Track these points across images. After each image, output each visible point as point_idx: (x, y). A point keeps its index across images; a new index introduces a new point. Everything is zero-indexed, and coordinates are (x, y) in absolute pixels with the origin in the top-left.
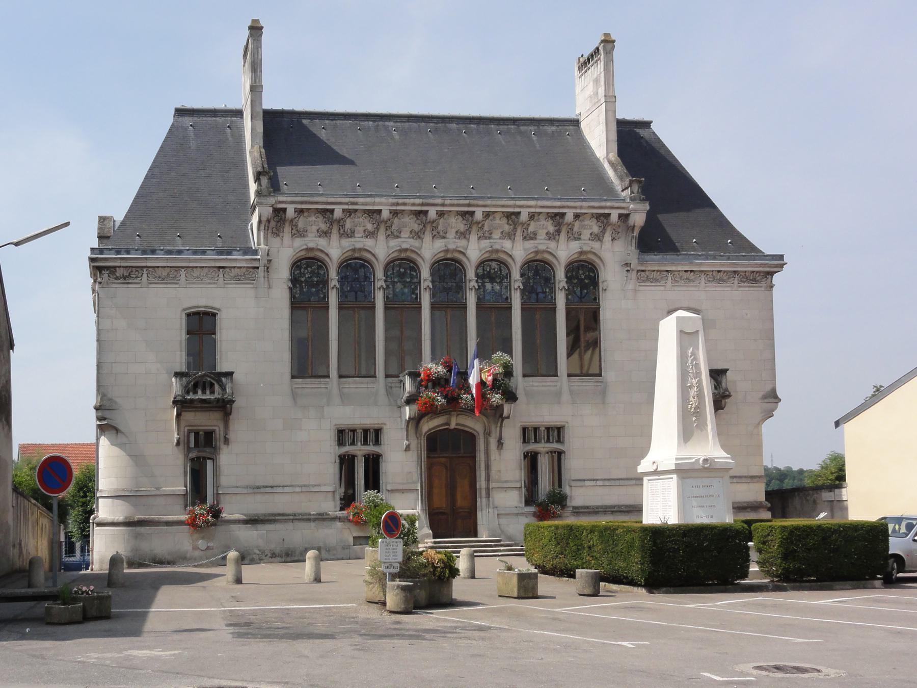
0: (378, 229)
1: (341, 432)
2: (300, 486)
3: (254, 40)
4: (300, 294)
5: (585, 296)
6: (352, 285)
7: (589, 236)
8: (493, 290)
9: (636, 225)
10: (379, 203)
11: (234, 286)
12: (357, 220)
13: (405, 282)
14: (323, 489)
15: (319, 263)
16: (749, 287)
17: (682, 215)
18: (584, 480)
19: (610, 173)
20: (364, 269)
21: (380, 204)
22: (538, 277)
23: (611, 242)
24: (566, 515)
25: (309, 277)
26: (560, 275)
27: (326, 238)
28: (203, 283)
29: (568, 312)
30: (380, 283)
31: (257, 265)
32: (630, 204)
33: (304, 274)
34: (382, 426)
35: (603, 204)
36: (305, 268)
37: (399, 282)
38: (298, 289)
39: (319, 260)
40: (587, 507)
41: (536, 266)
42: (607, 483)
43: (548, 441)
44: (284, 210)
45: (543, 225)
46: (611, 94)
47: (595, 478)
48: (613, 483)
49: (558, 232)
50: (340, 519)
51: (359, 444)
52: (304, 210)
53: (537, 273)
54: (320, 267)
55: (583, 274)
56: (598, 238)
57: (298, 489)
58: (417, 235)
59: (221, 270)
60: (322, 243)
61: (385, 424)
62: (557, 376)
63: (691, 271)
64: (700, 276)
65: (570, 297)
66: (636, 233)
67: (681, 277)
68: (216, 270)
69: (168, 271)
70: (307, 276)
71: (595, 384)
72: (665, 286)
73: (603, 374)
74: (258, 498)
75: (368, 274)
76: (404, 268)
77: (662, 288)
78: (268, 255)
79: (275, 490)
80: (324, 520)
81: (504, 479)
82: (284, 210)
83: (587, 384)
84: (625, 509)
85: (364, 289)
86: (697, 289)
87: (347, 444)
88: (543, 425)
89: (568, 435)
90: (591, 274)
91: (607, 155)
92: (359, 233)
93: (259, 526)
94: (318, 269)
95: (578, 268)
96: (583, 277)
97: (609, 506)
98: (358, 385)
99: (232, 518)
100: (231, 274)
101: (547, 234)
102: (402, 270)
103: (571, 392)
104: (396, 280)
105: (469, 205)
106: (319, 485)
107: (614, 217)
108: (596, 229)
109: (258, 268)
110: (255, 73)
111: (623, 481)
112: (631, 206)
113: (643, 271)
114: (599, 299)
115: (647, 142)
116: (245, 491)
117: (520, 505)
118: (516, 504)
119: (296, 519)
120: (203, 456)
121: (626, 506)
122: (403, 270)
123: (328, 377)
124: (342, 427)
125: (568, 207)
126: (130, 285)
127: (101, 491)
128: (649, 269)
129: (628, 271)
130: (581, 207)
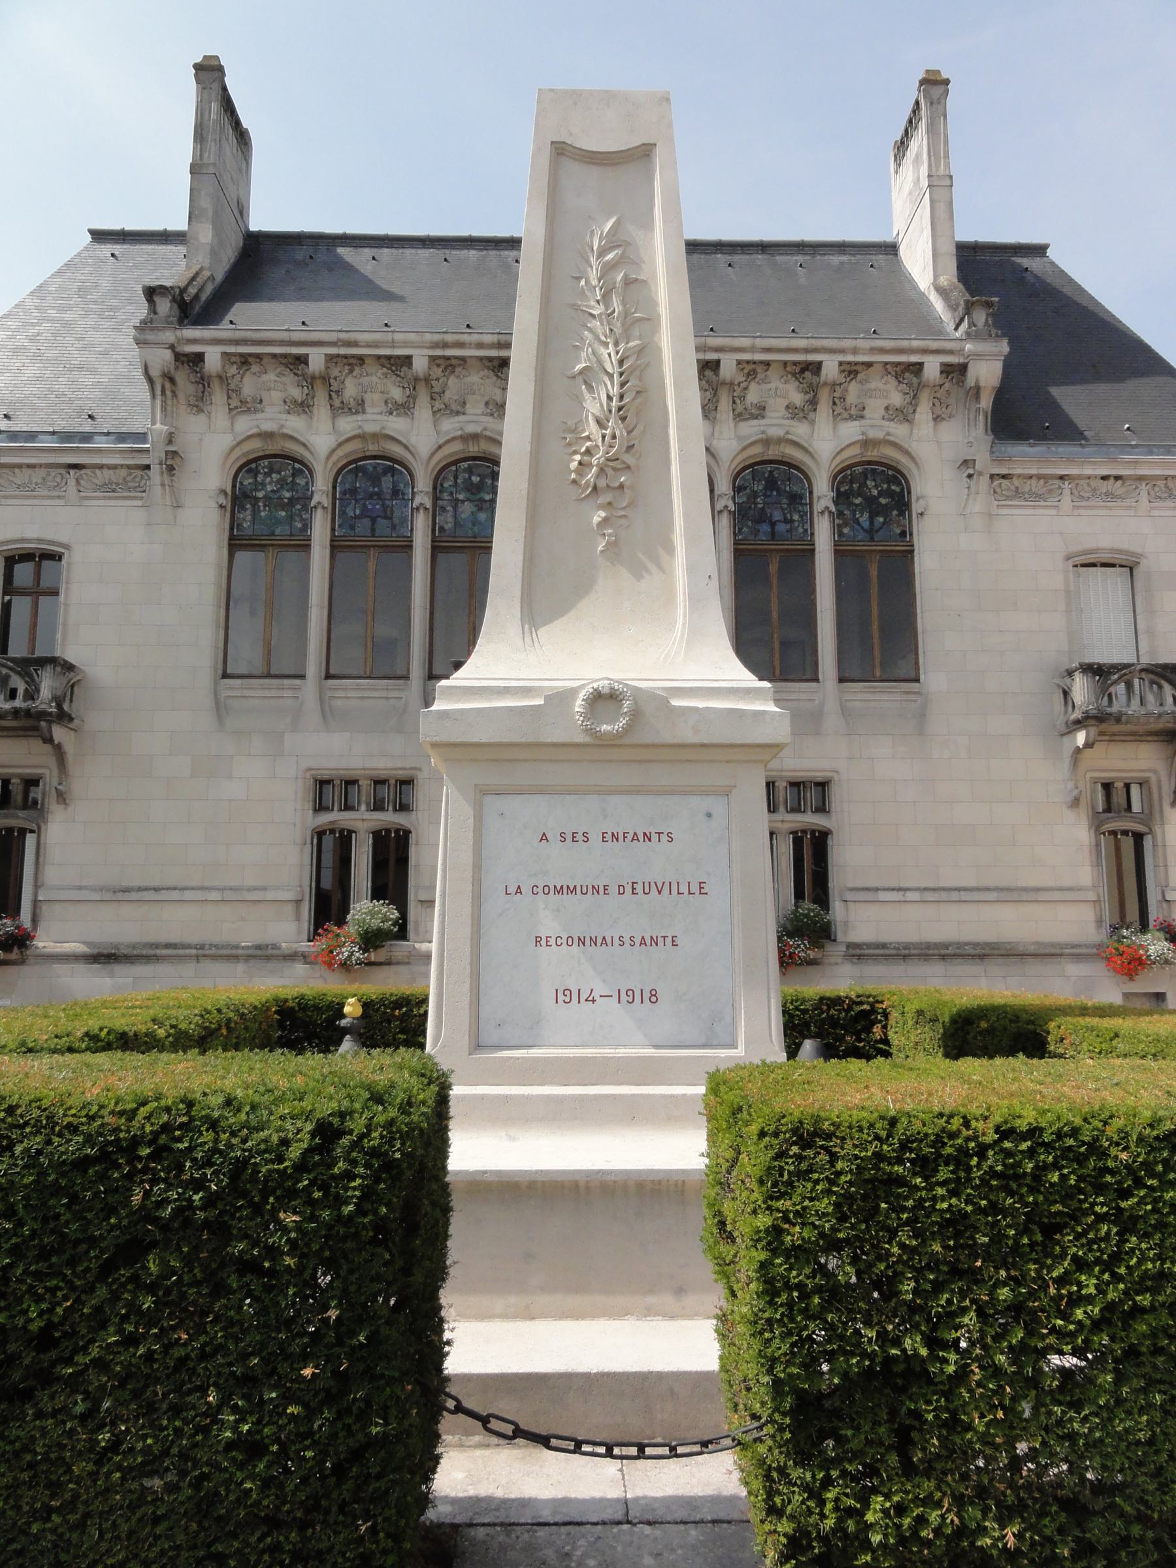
0: (412, 398)
1: (322, 784)
2: (219, 889)
3: (204, 88)
4: (253, 522)
6: (364, 505)
7: (883, 412)
9: (982, 384)
10: (405, 342)
11: (101, 502)
12: (365, 380)
13: (482, 500)
15: (297, 466)
17: (1102, 388)
18: (877, 889)
19: (938, 305)
20: (393, 476)
21: (406, 345)
22: (775, 493)
23: (931, 424)
24: (832, 960)
25: (273, 491)
26: (823, 491)
27: (303, 416)
28: (35, 497)
29: (839, 554)
30: (423, 498)
31: (147, 462)
32: (964, 343)
33: (263, 484)
34: (413, 772)
36: (265, 473)
37: (468, 500)
38: (248, 512)
39: (295, 460)
40: (884, 946)
41: (771, 472)
42: (930, 896)
43: (796, 809)
45: (776, 389)
46: (942, 171)
47: (904, 885)
48: (944, 896)
49: (813, 403)
50: (305, 957)
51: (363, 807)
52: (251, 360)
53: (772, 483)
54: (296, 473)
55: (876, 487)
56: (904, 415)
57: (215, 896)
59: (72, 472)
60: (295, 424)
61: (420, 769)
62: (817, 680)
63: (1117, 478)
64: (1137, 488)
65: (846, 530)
66: (986, 402)
67: (1094, 490)
68: (63, 471)
70: (269, 488)
71: (906, 697)
73: (922, 677)
74: (126, 910)
75: (402, 485)
77: (1053, 512)
78: (170, 442)
79: (163, 895)
80: (269, 958)
84: (972, 952)
85: (392, 512)
88: (782, 778)
89: (837, 796)
90: (893, 487)
91: (936, 277)
92: (373, 405)
93: (118, 968)
94: (293, 475)
95: (865, 475)
96: (875, 492)
97: (935, 944)
98: (367, 694)
99: (59, 950)
100: (95, 481)
101: (788, 407)
102: (475, 479)
103: (845, 712)
104: (461, 497)
106: (264, 889)
107: (932, 368)
108: (897, 399)
109: (148, 467)
110: (201, 142)
112: (968, 347)
113: (1004, 477)
114: (911, 534)
115: (1035, 276)
116: (97, 896)
119: (204, 956)
120: (8, 825)
121: (975, 945)
123: (302, 677)
124: (326, 775)
125: (925, 351)
128: (1019, 471)
129: (970, 476)
130: (855, 351)
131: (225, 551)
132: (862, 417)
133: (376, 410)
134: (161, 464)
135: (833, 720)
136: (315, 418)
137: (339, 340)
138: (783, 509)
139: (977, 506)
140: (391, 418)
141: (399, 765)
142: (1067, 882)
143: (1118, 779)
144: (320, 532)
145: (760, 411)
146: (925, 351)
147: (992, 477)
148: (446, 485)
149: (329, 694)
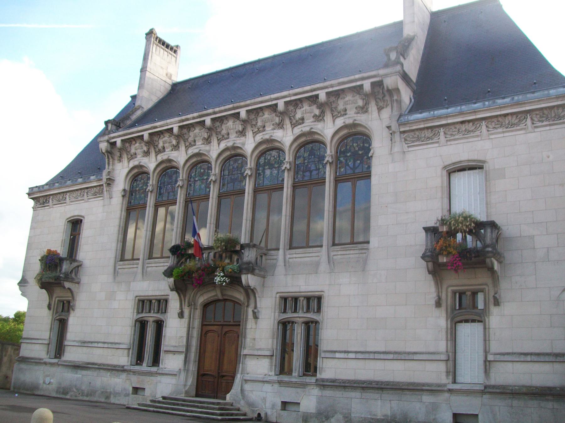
5: (358, 166)
8: (271, 174)
14: (121, 346)
16: (550, 125)
18: (335, 352)
26: (330, 152)
31: (101, 183)
35: (352, 78)
44: (115, 142)
48: (367, 356)
58: (242, 133)
69: (99, 189)
70: (140, 186)
71: (361, 251)
72: (525, 128)
76: (203, 169)
77: (437, 145)
81: (257, 347)
82: (115, 142)
83: (352, 254)
86: (479, 139)
87: (152, 312)
89: (325, 303)
90: (365, 145)
98: (158, 265)
104: (197, 179)
105: (234, 108)
109: (102, 185)
111: (379, 355)
117: (270, 373)
118: (266, 372)
122: (203, 170)
125: (363, 79)
126: (46, 208)
127: (167, 346)
130: (332, 86)
131: (124, 213)
132: (346, 114)
133: (169, 150)
134: (105, 183)
135: (324, 266)
136: (151, 157)
137: (152, 127)
138: (315, 164)
139: (397, 148)
140: (173, 152)
141: (163, 294)
142: (432, 350)
143: (468, 290)
144: (329, 174)
145: (344, 112)
146: (363, 79)
147: (401, 132)
148: (192, 175)
149: (332, 254)
